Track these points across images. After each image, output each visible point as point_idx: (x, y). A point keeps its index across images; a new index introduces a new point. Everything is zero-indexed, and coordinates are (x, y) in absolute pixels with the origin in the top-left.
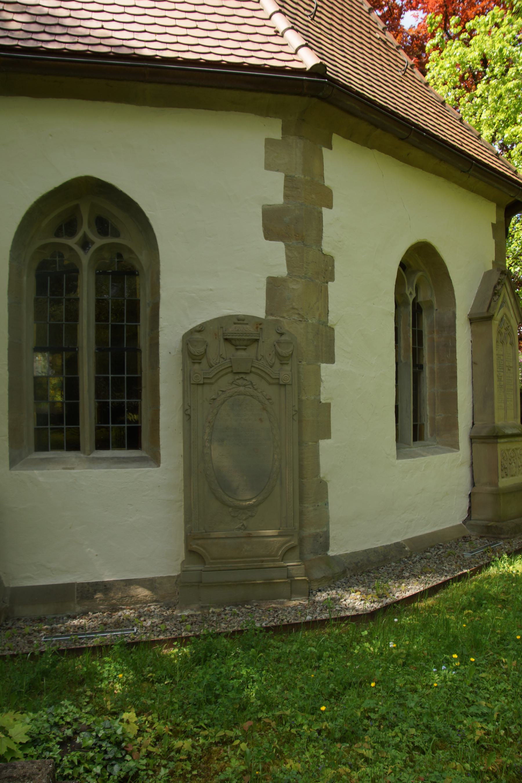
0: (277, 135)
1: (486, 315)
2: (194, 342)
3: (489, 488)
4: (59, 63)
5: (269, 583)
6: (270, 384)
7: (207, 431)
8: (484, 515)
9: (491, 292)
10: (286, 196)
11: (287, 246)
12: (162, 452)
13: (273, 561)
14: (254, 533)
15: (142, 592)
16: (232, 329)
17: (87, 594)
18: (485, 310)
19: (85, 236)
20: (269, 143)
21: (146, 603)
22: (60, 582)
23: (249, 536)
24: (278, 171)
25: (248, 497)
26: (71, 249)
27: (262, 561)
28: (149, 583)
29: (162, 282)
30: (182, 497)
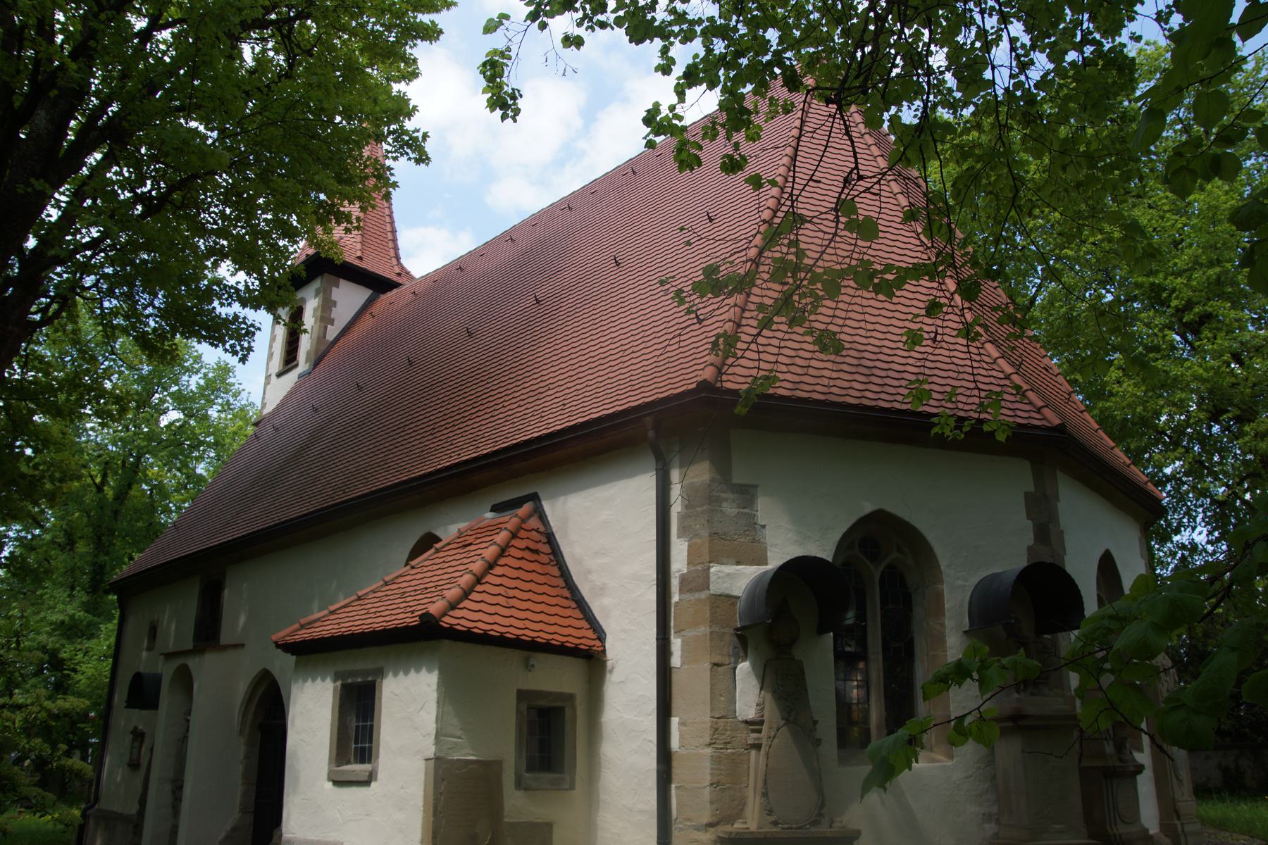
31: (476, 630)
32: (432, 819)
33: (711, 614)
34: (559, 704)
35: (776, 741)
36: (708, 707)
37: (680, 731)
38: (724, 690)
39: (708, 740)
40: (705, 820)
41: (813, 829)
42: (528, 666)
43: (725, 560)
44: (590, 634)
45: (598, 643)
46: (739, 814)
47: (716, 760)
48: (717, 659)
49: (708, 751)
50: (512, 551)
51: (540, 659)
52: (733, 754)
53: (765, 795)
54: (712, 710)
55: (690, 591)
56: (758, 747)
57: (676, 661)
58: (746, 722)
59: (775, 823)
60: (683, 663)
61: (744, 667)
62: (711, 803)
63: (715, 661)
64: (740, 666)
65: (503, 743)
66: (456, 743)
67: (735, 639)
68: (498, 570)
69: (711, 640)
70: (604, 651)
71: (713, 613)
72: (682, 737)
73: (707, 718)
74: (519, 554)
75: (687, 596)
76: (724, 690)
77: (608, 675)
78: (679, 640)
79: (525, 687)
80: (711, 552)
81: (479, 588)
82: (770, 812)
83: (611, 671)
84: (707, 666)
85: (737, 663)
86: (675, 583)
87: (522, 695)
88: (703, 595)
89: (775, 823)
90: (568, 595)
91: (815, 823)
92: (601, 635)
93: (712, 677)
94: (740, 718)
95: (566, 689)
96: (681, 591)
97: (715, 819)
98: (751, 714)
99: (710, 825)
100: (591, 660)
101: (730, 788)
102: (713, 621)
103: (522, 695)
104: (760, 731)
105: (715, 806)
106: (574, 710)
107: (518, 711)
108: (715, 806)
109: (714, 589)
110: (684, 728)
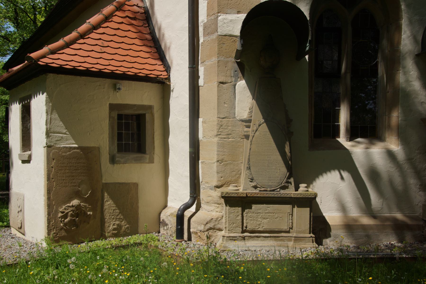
31: (140, 74)
32: (47, 182)
33: (219, 48)
34: (141, 112)
35: (257, 133)
36: (216, 112)
37: (203, 127)
38: (227, 100)
39: (215, 133)
40: (215, 183)
41: (282, 192)
42: (116, 88)
43: (229, 11)
44: (161, 68)
45: (165, 73)
46: (236, 181)
47: (221, 146)
48: (222, 79)
49: (216, 139)
50: (115, 19)
51: (125, 85)
52: (233, 141)
53: (249, 168)
54: (218, 113)
55: (208, 34)
56: (247, 137)
57: (201, 82)
58: (242, 121)
59: (255, 187)
60: (204, 83)
61: (242, 84)
62: (218, 173)
63: (221, 80)
64: (238, 83)
65: (102, 138)
66: (62, 137)
67: (236, 65)
68: (101, 30)
69: (218, 66)
70: (169, 79)
71: (220, 48)
72: (204, 131)
73: (215, 119)
74: (120, 20)
75: (207, 38)
76: (227, 100)
77: (171, 93)
78: (203, 68)
79: (111, 102)
80: (219, 6)
81: (82, 41)
82: (252, 180)
83: (173, 91)
84: (216, 84)
85: (236, 81)
86: (201, 29)
87: (112, 107)
88: (214, 36)
89: (255, 187)
90: (152, 45)
91: (284, 188)
92: (168, 69)
93: (219, 91)
94: (238, 118)
95: (146, 102)
96: (204, 35)
97: (220, 184)
98: (245, 115)
99: (218, 187)
100: (163, 85)
101: (231, 164)
102: (219, 54)
103: (112, 107)
104: (248, 127)
105: (220, 175)
106: (153, 115)
107: (110, 117)
108: (220, 175)
109: (221, 31)
110: (205, 125)
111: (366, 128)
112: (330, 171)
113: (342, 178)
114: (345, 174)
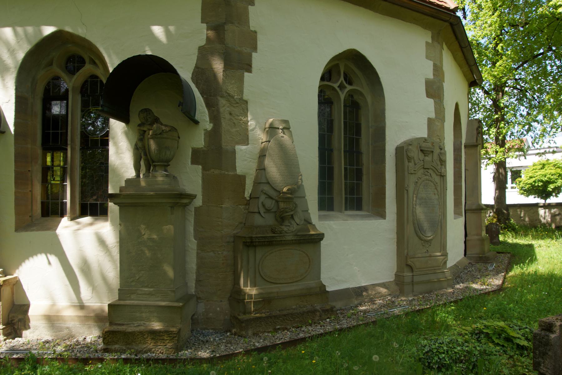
0: (430, 41)
1: (476, 144)
2: (400, 151)
3: (476, 237)
4: (420, 6)
5: (439, 281)
6: (437, 175)
7: (415, 199)
8: (474, 251)
9: (475, 132)
10: (434, 75)
11: (435, 101)
12: (387, 211)
13: (439, 269)
14: (432, 254)
15: (383, 290)
16: (424, 145)
17: (359, 292)
18: (475, 141)
19: (342, 83)
20: (427, 43)
21: (385, 296)
22: (342, 288)
23: (430, 256)
24: (431, 60)
25: (430, 235)
26: (334, 89)
27: (435, 270)
28: (383, 285)
29: (386, 115)
30: (396, 237)
111: (92, 206)
112: (36, 254)
113: (50, 263)
114: (53, 259)
